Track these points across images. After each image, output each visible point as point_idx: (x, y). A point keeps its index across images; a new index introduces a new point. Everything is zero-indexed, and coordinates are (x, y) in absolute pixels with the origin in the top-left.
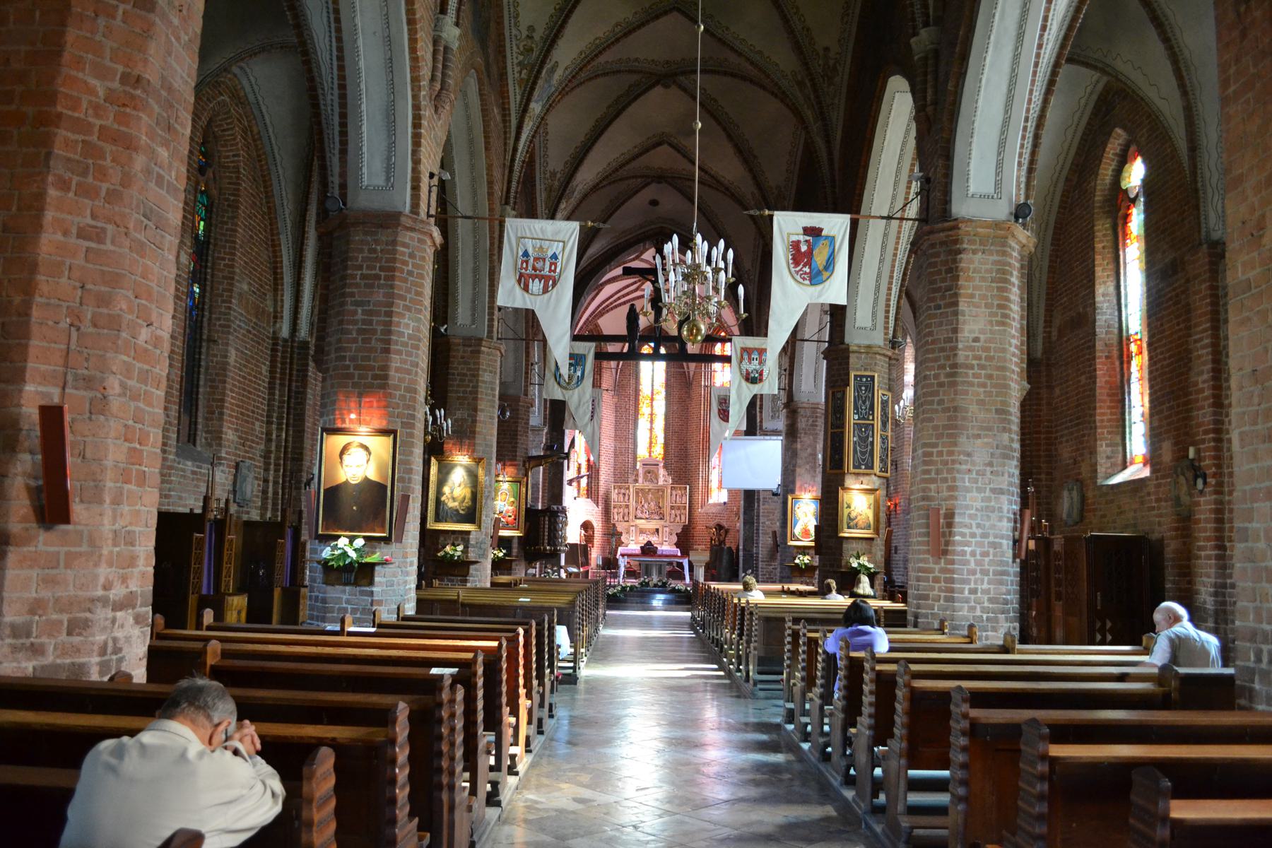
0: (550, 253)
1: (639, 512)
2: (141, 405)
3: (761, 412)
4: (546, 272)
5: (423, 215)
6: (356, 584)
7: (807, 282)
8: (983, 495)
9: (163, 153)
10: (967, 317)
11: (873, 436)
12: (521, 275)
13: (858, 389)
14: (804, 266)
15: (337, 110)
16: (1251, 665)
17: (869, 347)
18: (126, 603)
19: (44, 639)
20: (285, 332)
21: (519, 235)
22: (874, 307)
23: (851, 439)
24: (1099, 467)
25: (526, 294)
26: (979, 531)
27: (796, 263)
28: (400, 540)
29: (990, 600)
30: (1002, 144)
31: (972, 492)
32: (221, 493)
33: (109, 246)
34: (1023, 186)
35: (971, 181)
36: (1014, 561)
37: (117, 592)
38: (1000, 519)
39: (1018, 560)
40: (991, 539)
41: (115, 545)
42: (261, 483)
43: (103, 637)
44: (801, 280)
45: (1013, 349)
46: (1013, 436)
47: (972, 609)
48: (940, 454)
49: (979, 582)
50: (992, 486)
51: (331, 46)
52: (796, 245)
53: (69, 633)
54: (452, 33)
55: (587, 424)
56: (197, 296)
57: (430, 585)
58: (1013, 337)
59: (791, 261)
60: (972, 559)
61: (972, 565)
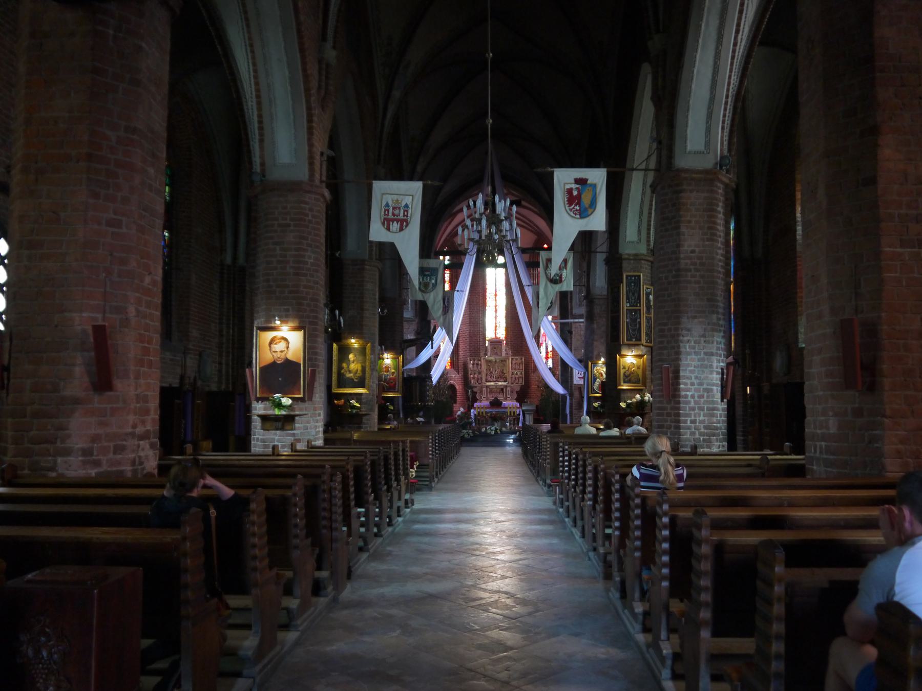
0: (403, 204)
1: (488, 377)
2: (148, 321)
3: (571, 302)
4: (401, 216)
5: (317, 182)
6: (282, 429)
7: (578, 216)
8: (699, 357)
9: (152, 171)
10: (686, 237)
11: (640, 318)
12: (385, 219)
13: (628, 285)
14: (576, 205)
15: (256, 113)
16: (812, 455)
17: (636, 255)
18: (144, 436)
19: (101, 457)
20: (229, 260)
21: (383, 192)
22: (639, 227)
23: (624, 320)
24: (799, 334)
25: (388, 232)
26: (696, 381)
27: (570, 204)
28: (310, 399)
29: (705, 427)
30: (710, 116)
31: (691, 354)
32: (191, 373)
33: (124, 230)
34: (726, 143)
35: (688, 142)
36: (722, 401)
37: (140, 430)
38: (711, 373)
39: (725, 400)
40: (705, 386)
41: (138, 402)
42: (217, 365)
43: (133, 455)
44: (574, 215)
45: (719, 257)
46: (720, 316)
47: (693, 434)
48: (670, 330)
49: (697, 415)
50: (705, 350)
51: (249, 68)
52: (570, 191)
53: (115, 453)
54: (331, 54)
55: (440, 317)
56: (167, 238)
57: (334, 430)
58: (720, 248)
59: (566, 203)
60: (692, 400)
61: (692, 404)
